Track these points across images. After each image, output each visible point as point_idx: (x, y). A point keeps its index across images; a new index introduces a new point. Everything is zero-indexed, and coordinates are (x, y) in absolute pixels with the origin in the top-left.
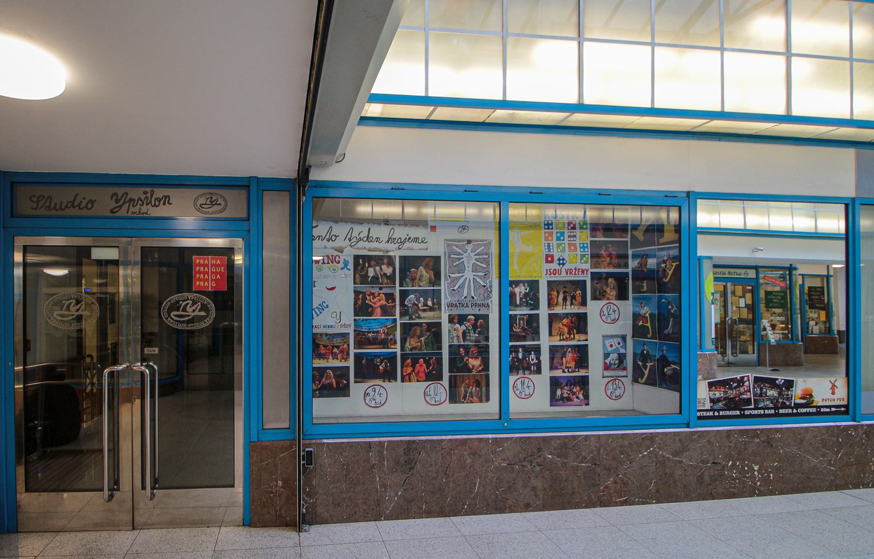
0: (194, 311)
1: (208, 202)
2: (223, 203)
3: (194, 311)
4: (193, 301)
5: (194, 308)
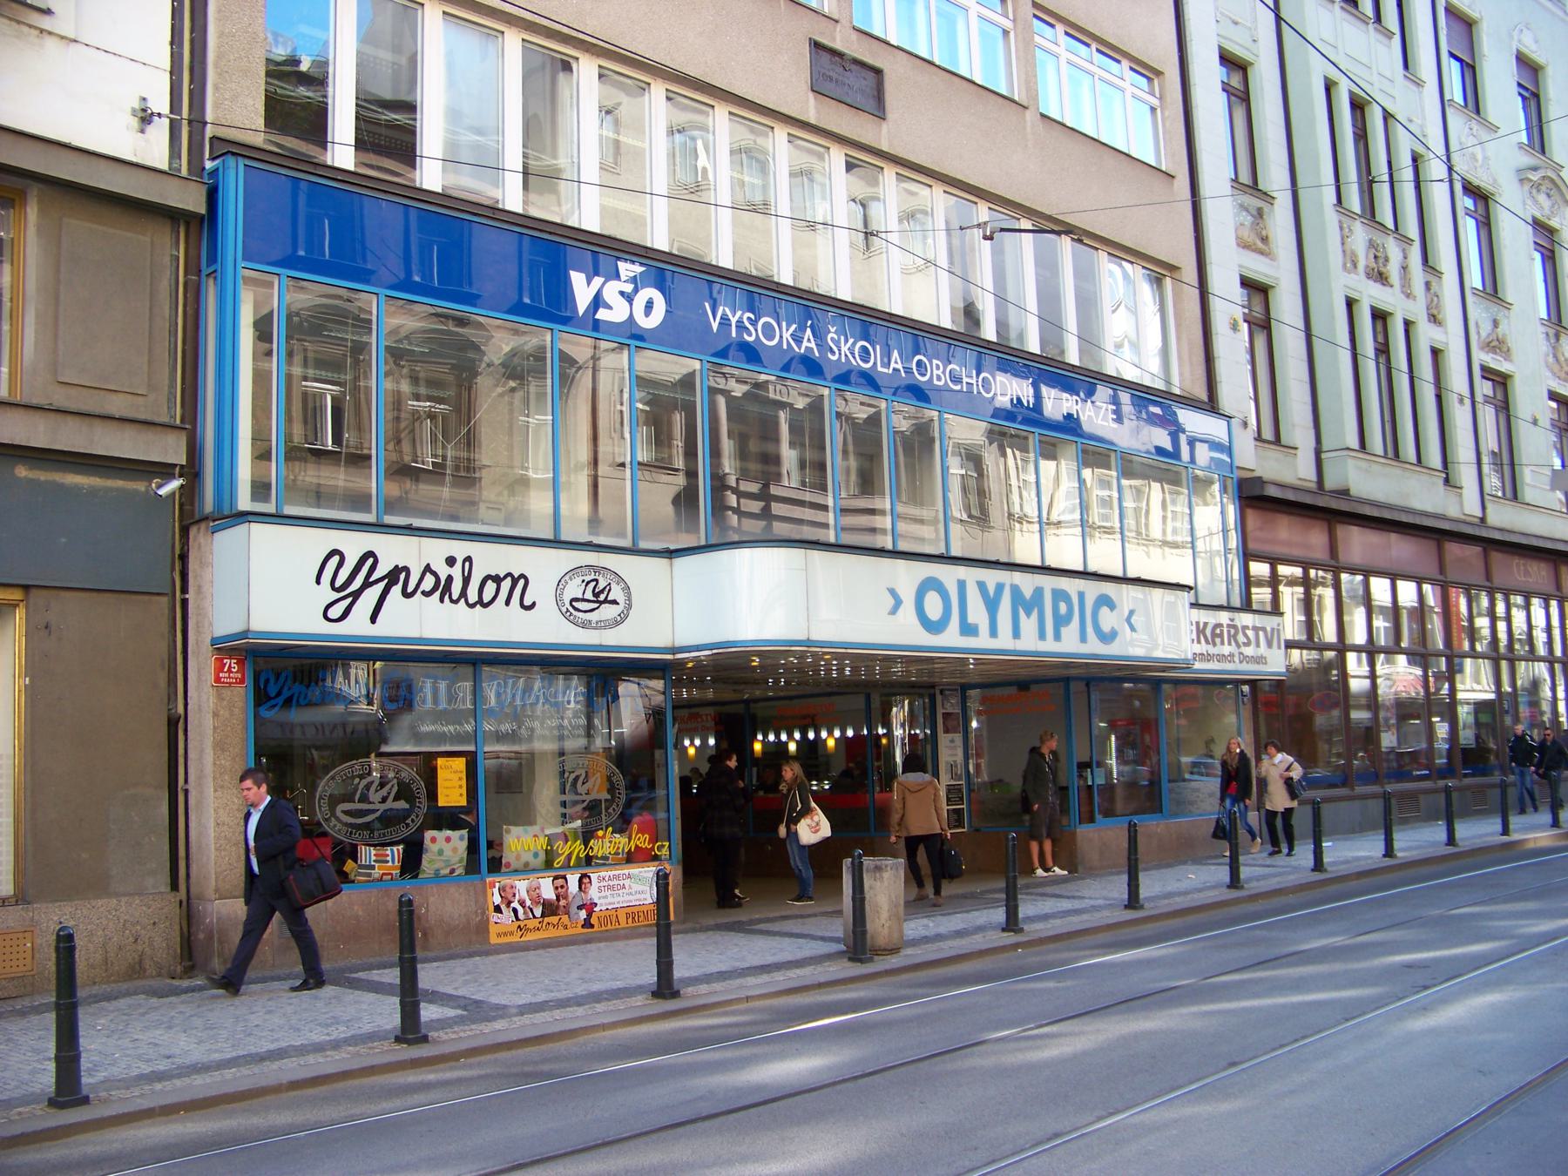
0: (384, 800)
2: (620, 597)
3: (384, 800)
5: (384, 792)
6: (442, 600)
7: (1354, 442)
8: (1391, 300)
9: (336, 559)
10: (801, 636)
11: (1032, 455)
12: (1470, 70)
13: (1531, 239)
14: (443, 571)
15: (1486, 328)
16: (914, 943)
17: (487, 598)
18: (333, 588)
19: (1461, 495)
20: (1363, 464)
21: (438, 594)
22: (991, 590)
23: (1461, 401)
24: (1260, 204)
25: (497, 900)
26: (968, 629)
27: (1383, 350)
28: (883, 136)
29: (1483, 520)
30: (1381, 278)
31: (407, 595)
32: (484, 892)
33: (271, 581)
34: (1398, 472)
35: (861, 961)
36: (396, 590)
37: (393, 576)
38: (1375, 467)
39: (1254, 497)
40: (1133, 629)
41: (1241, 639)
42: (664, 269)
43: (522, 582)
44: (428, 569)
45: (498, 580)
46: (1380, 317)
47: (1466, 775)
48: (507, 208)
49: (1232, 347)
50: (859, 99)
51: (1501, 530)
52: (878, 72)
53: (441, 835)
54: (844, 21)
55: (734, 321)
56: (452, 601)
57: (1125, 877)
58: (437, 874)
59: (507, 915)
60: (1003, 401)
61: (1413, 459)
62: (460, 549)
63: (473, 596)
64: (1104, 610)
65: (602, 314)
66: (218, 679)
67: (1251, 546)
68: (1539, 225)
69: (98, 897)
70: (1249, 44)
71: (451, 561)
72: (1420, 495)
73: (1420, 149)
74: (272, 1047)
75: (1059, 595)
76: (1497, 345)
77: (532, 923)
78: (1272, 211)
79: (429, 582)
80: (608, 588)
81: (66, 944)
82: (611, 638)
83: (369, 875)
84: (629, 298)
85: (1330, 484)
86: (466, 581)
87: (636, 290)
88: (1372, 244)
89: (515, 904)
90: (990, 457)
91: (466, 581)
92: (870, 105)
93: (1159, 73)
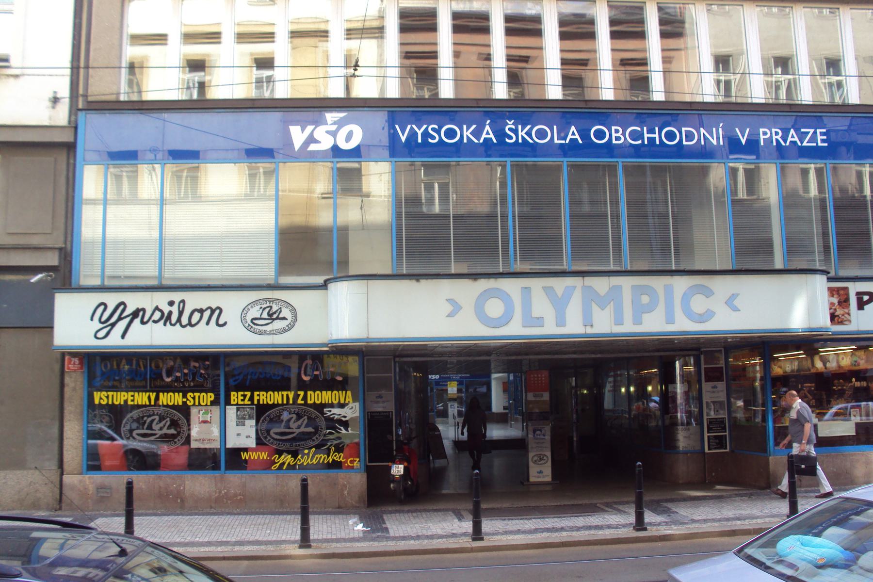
0: (299, 427)
1: (265, 315)
3: (299, 427)
4: (160, 416)
6: (165, 325)
9: (102, 307)
14: (166, 309)
17: (194, 321)
18: (101, 322)
21: (162, 322)
31: (143, 323)
36: (137, 321)
37: (135, 314)
43: (217, 312)
44: (157, 308)
45: (201, 311)
48: (532, 98)
55: (420, 132)
56: (171, 324)
62: (177, 297)
63: (185, 320)
69: (20, 469)
74: (192, 540)
79: (157, 315)
81: (130, 486)
86: (181, 313)
91: (181, 313)
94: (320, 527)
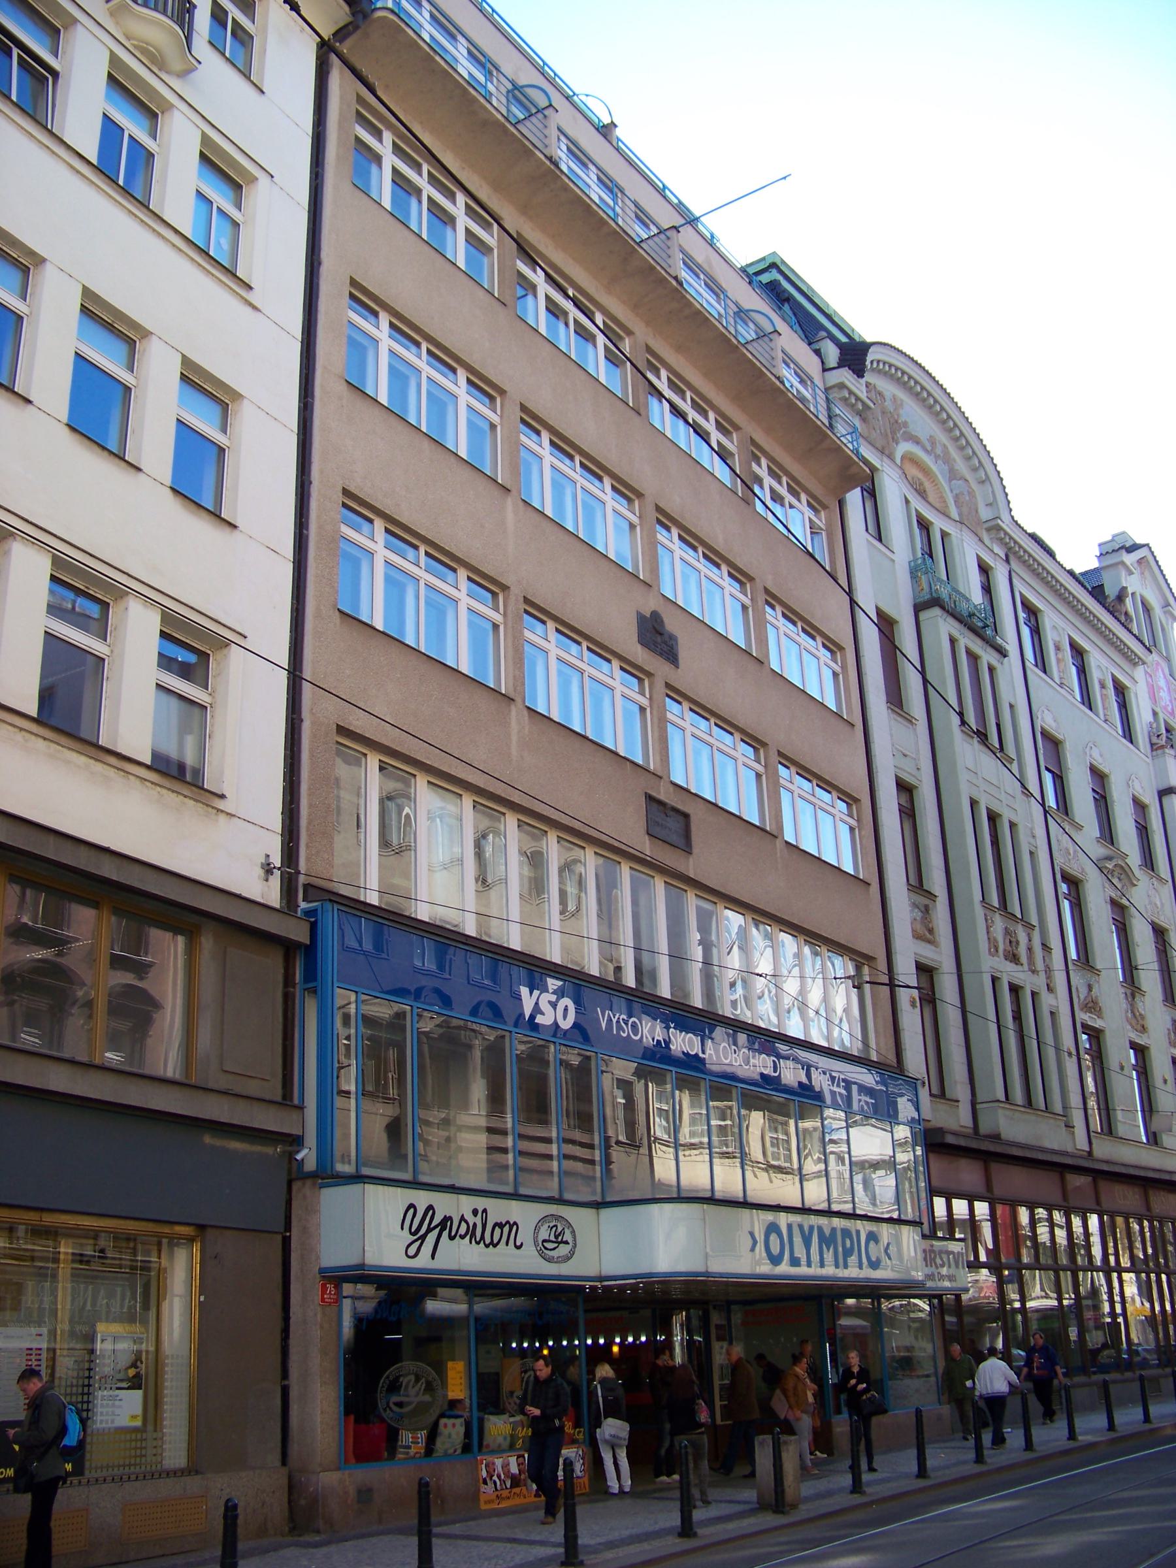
1: (552, 1238)
3: (417, 1394)
7: (1001, 1095)
8: (1021, 976)
9: (412, 1210)
10: (701, 1269)
11: (669, 1086)
12: (1060, 780)
13: (1110, 916)
14: (471, 1219)
15: (1083, 992)
16: (807, 1499)
18: (411, 1233)
19: (1073, 1133)
20: (1008, 1113)
22: (806, 1229)
23: (1070, 1054)
24: (927, 902)
25: (484, 1474)
26: (795, 1262)
27: (1018, 1016)
28: (691, 867)
29: (1090, 1153)
30: (1014, 958)
32: (477, 1469)
33: (372, 1228)
34: (1033, 1118)
35: (783, 1513)
36: (445, 1234)
38: (1017, 1114)
39: (933, 1142)
40: (890, 1258)
41: (939, 1261)
42: (576, 982)
44: (462, 1219)
45: (501, 1225)
46: (1015, 989)
47: (1094, 1373)
49: (911, 1020)
50: (674, 838)
51: (1107, 1162)
52: (686, 816)
53: (449, 1422)
54: (519, 700)
55: (614, 1020)
57: (915, 1451)
58: (446, 1455)
59: (490, 1484)
60: (648, 1041)
61: (1043, 1107)
64: (872, 1244)
65: (539, 1019)
66: (323, 1300)
67: (935, 1183)
68: (1114, 903)
70: (914, 772)
71: (475, 1212)
72: (1050, 1138)
73: (1033, 849)
75: (846, 1233)
76: (1092, 1006)
77: (505, 1493)
78: (935, 906)
80: (563, 1232)
82: (565, 1269)
83: (407, 1453)
84: (554, 1005)
85: (984, 1129)
87: (558, 1000)
88: (1007, 932)
89: (495, 1478)
90: (639, 1087)
92: (681, 842)
93: (856, 800)
94: (936, 1457)
